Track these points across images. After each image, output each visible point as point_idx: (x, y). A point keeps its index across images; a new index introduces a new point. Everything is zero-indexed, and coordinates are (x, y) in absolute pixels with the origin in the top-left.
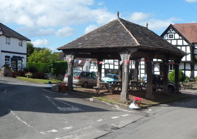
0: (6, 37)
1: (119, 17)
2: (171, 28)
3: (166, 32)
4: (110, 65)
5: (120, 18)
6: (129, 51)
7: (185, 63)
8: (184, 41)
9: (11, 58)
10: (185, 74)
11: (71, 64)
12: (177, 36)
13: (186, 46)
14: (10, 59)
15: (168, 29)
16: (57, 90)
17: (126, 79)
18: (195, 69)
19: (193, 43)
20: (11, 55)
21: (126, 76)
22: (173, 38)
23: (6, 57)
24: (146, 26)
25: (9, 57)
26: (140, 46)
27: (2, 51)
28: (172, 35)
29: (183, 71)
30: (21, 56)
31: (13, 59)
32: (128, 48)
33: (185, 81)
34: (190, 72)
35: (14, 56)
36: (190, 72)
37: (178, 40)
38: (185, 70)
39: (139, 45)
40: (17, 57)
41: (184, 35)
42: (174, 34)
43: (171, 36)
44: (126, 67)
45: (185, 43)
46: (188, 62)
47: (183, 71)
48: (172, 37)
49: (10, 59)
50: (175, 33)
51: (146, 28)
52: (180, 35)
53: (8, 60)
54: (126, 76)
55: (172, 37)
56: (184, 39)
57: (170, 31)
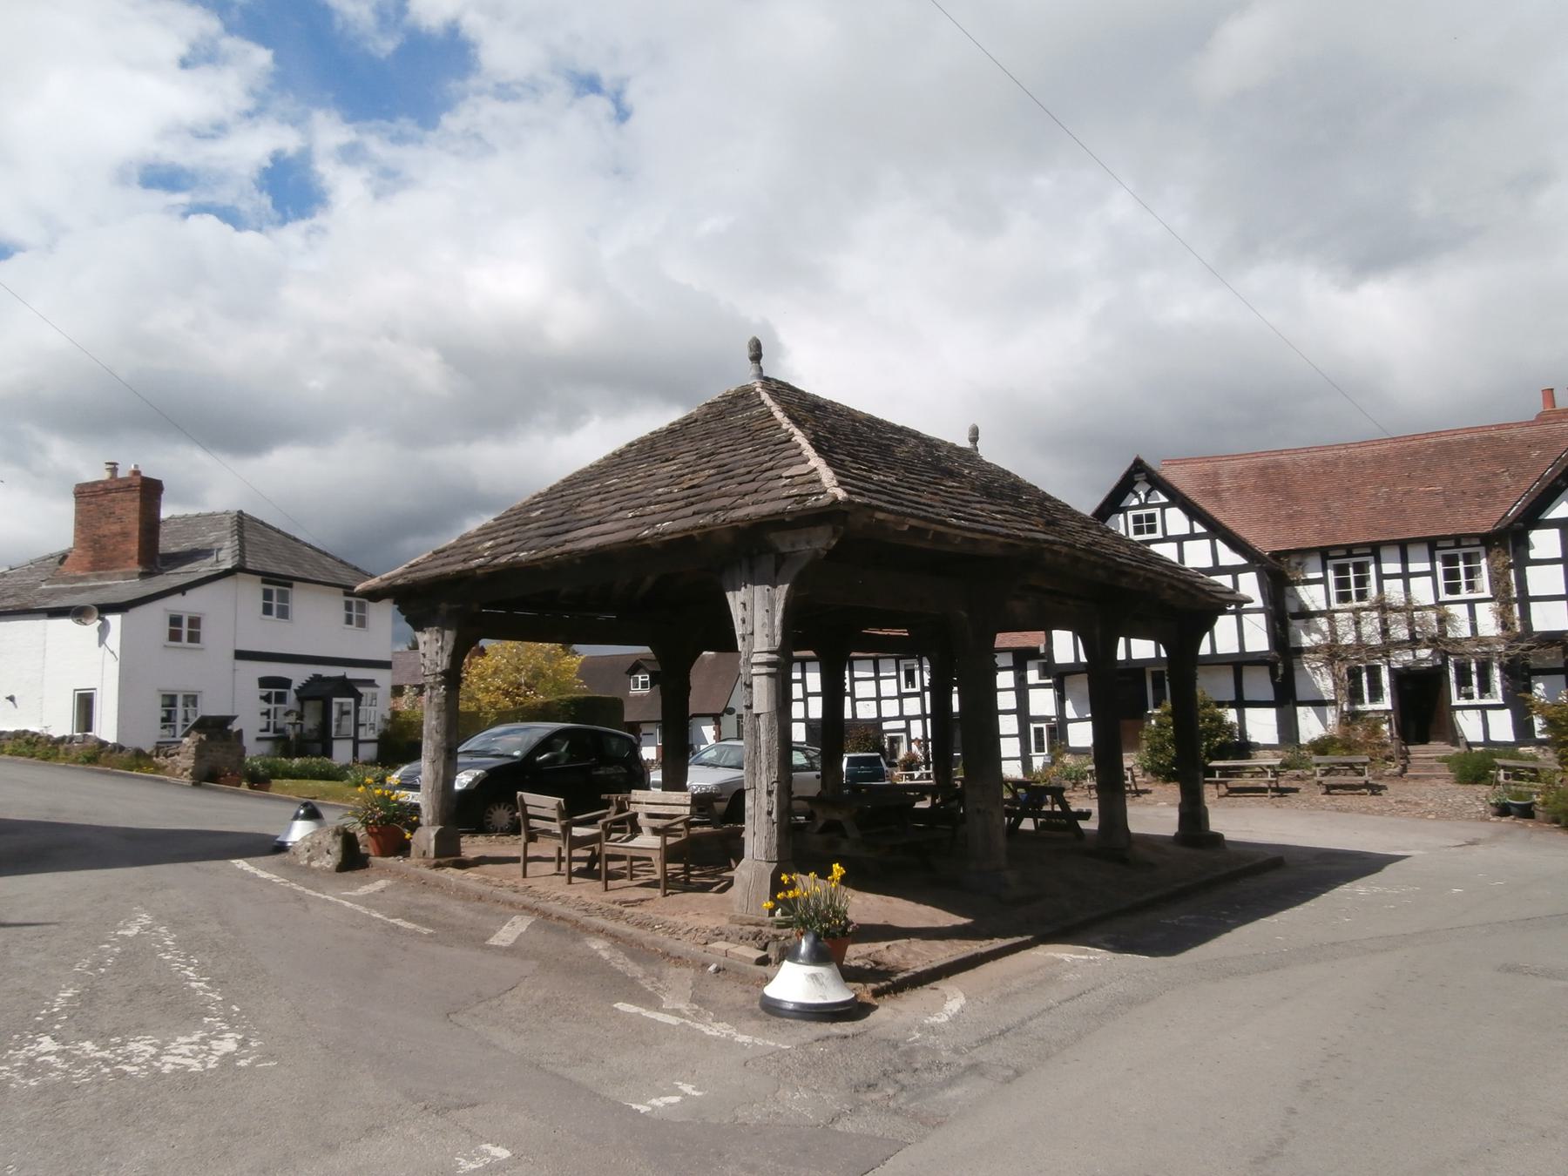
0: (264, 582)
1: (761, 369)
2: (1138, 477)
3: (1113, 504)
4: (1429, 578)
5: (767, 379)
6: (783, 555)
7: (1240, 663)
8: (1222, 547)
9: (295, 686)
10: (1191, 521)
11: (441, 683)
12: (1177, 521)
13: (1234, 571)
14: (291, 696)
15: (1125, 486)
16: (330, 861)
17: (764, 766)
18: (1299, 698)
19: (1276, 555)
20: (298, 675)
21: (763, 737)
22: (1159, 535)
23: (265, 682)
24: (967, 444)
25: (285, 683)
26: (849, 502)
27: (241, 655)
28: (1151, 518)
29: (1231, 715)
30: (353, 673)
31: (305, 693)
32: (772, 536)
33: (441, 683)
34: (1270, 715)
35: (317, 679)
36: (1270, 715)
37: (1186, 544)
38: (1240, 704)
39: (841, 494)
40: (329, 679)
41: (1220, 516)
42: (1157, 511)
43: (1145, 524)
44: (764, 670)
45: (1228, 557)
46: (1256, 660)
47: (1231, 715)
48: (1152, 529)
49: (291, 696)
50: (1163, 507)
51: (969, 456)
52: (1193, 512)
53: (281, 698)
54: (763, 737)
55: (1152, 529)
56: (1216, 531)
57: (1137, 496)
